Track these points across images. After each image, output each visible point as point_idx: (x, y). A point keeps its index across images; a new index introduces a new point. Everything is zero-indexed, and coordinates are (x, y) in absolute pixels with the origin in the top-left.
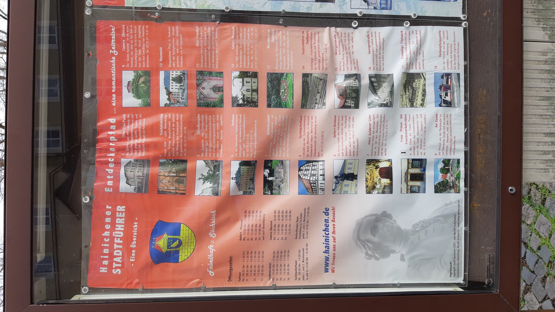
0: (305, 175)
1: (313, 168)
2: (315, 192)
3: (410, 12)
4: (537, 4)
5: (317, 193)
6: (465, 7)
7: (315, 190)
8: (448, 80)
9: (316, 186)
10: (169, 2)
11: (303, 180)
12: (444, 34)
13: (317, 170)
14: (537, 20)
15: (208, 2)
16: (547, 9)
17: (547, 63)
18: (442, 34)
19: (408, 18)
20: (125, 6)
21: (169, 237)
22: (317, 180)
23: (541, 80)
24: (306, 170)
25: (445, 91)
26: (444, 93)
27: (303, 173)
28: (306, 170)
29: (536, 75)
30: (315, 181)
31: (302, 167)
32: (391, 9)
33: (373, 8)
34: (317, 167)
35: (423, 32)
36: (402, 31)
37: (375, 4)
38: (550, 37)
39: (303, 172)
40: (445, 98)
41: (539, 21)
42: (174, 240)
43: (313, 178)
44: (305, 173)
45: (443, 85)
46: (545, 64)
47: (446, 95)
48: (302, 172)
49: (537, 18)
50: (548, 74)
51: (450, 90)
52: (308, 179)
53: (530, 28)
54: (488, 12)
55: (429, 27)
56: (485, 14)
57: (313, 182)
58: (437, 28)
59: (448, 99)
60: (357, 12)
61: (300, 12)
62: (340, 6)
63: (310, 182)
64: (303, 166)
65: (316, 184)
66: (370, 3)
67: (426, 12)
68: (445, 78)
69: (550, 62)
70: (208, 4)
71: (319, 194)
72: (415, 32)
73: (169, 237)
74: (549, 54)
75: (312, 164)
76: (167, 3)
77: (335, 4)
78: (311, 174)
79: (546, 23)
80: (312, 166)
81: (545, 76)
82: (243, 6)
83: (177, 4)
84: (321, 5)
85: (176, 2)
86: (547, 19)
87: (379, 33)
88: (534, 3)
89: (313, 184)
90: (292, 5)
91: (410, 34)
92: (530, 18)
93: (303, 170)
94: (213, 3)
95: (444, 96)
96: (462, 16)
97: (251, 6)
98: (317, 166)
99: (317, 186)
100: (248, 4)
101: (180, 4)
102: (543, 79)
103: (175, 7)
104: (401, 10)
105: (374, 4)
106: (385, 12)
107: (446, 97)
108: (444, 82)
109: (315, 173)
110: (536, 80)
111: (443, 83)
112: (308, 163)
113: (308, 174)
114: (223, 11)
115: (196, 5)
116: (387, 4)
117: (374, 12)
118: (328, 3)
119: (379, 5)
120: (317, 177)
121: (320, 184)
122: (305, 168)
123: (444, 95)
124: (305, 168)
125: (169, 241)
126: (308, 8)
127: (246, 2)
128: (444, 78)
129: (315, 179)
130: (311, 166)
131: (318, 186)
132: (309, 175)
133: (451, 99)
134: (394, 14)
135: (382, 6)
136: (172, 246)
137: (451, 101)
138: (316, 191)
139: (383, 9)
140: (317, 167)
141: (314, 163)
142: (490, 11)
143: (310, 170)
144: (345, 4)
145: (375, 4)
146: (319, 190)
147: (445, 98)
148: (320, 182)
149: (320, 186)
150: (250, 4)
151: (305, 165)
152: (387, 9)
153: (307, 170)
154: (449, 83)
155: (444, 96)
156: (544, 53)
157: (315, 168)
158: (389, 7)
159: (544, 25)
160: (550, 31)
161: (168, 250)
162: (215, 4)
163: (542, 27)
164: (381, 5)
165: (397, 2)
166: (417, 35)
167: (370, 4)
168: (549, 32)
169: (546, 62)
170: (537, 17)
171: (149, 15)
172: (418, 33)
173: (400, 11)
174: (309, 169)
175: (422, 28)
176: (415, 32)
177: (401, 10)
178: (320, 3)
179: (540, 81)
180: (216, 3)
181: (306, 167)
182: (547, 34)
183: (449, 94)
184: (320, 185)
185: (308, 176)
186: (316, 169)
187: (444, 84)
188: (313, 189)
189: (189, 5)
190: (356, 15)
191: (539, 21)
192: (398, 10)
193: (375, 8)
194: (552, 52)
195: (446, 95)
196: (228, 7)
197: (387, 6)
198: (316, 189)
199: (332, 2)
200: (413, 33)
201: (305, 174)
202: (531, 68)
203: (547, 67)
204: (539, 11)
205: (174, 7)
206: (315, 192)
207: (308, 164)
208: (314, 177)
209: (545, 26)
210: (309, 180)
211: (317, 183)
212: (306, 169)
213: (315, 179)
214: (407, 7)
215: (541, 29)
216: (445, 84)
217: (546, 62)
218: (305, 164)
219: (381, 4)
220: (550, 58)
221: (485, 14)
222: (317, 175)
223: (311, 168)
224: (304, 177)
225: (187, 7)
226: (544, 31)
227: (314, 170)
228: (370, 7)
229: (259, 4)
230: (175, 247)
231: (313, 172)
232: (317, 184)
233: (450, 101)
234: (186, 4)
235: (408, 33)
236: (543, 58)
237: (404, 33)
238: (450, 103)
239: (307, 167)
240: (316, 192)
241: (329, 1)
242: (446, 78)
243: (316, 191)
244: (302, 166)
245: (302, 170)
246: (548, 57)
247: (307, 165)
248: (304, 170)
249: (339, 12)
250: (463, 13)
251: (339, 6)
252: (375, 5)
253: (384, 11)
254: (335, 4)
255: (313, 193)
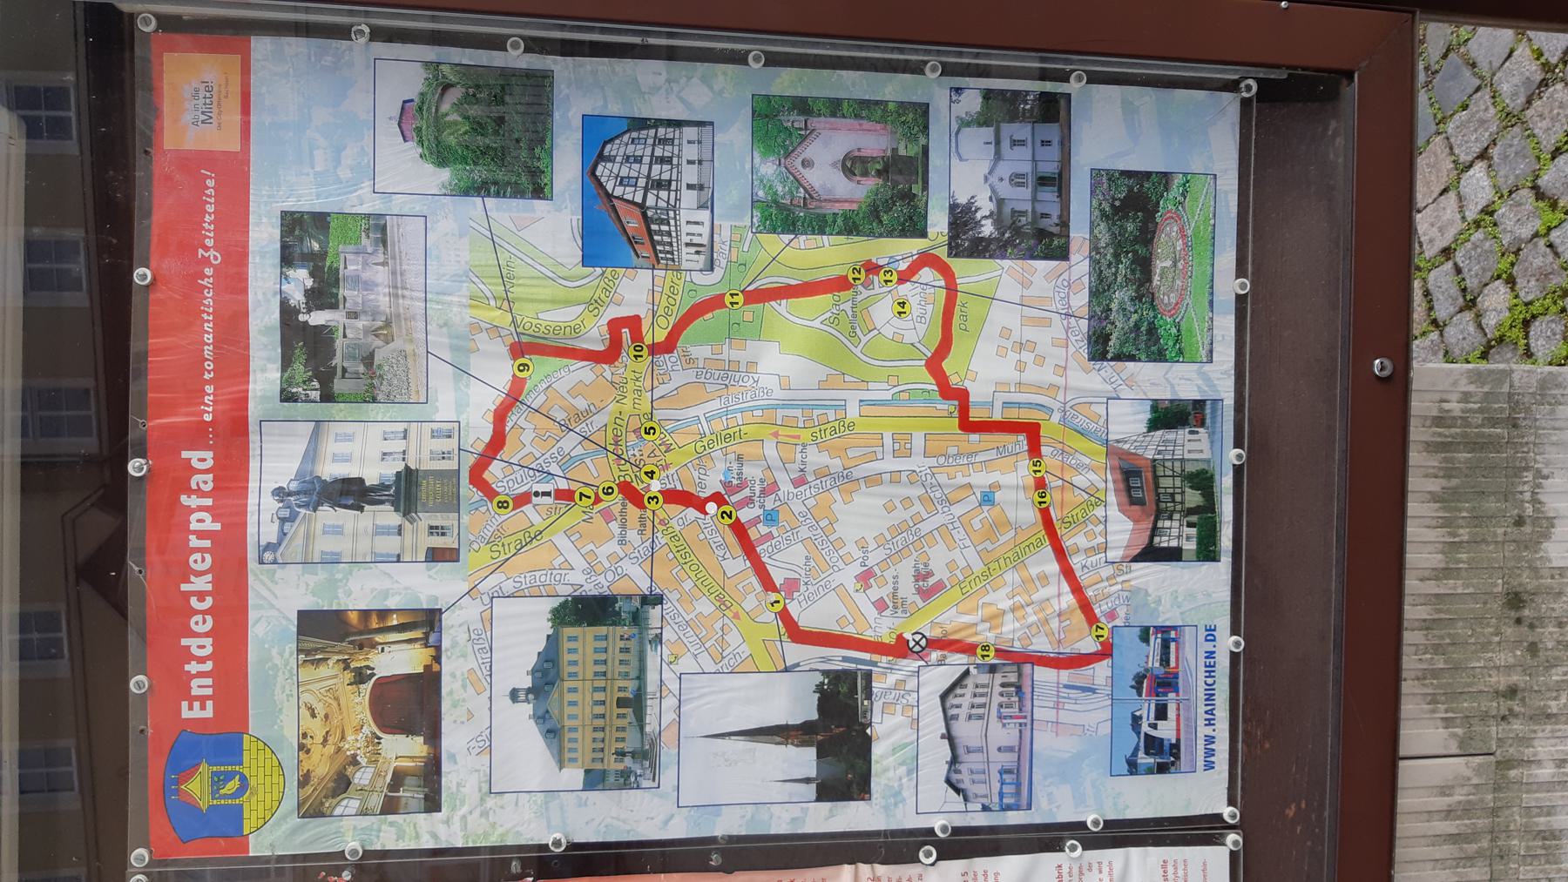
0: (622, 181)
1: (658, 152)
2: (667, 259)
3: (1083, 812)
4: (1431, 654)
5: (673, 260)
6: (1236, 782)
7: (667, 248)
8: (1169, 648)
9: (669, 234)
10: (382, 834)
11: (616, 202)
12: (1176, 868)
13: (675, 161)
14: (1429, 698)
15: (501, 826)
16: (1456, 668)
17: (1452, 814)
18: (1170, 870)
19: (1076, 829)
20: (251, 854)
21: (215, 769)
22: (674, 208)
23: (1432, 863)
24: (627, 158)
25: (1157, 696)
26: (1153, 707)
27: (615, 171)
28: (627, 158)
29: (1422, 851)
30: (667, 210)
31: (608, 147)
32: (1029, 807)
33: (979, 807)
34: (676, 152)
35: (1117, 867)
36: (1060, 866)
37: (986, 796)
38: (1461, 744)
39: (617, 166)
40: (1154, 726)
41: (1434, 700)
42: (229, 777)
43: (657, 196)
44: (624, 172)
45: (1147, 670)
46: (1446, 818)
47: (1161, 713)
48: (609, 165)
49: (1429, 694)
50: (1454, 844)
51: (1177, 692)
52: (639, 199)
53: (1412, 722)
54: (1298, 807)
55: (1135, 852)
56: (1291, 812)
57: (656, 216)
58: (1156, 854)
59: (1166, 731)
60: (938, 824)
61: (772, 832)
62: (886, 808)
63: (644, 215)
64: (617, 141)
65: (668, 224)
66: (970, 794)
67: (1127, 807)
68: (1155, 641)
69: (1459, 813)
70: (500, 830)
71: (685, 265)
72: (1095, 866)
73: (215, 769)
74: (1458, 790)
75: (652, 132)
76: (378, 837)
77: (871, 806)
78: (648, 177)
79: (1455, 705)
80: (654, 145)
81: (1446, 851)
82: (604, 829)
83: (407, 837)
84: (831, 810)
85: (404, 831)
86: (1453, 696)
87: (997, 874)
88: (1424, 653)
89: (659, 224)
90: (749, 816)
91: (1081, 873)
92: (1411, 697)
93: (615, 157)
94: (515, 826)
95: (1152, 720)
96: (1227, 812)
97: (628, 828)
98: (673, 144)
99: (674, 234)
100: (621, 824)
101: (417, 837)
102: (1437, 860)
103: (402, 846)
104: (1058, 807)
105: (981, 797)
106: (1014, 818)
107: (1159, 722)
108: (1151, 658)
109: (666, 176)
110: (1421, 864)
111: (1147, 663)
112: (639, 129)
113: (637, 178)
114: (545, 847)
115: (466, 837)
116: (1018, 793)
117: (981, 820)
118: (852, 803)
119: (996, 799)
120: (673, 194)
121: (688, 222)
122: (622, 150)
123: (1152, 715)
124: (622, 150)
125: (216, 779)
126: (793, 819)
127: (613, 818)
128: (1152, 639)
129: (668, 202)
130: (650, 141)
131: (677, 231)
132: (642, 182)
133: (1178, 730)
134: (1038, 820)
135: (1005, 801)
136: (222, 792)
137: (1178, 740)
138: (668, 252)
139: (1008, 808)
140: (676, 152)
141: (661, 131)
142: (1303, 806)
143: (646, 160)
144: (901, 802)
145: (986, 796)
146: (685, 250)
147: (1154, 726)
148: (684, 216)
149: (688, 234)
150: (624, 821)
151: (626, 138)
152: (1016, 807)
153: (632, 160)
154: (1173, 664)
155: (1152, 720)
156: (1445, 790)
157: (666, 154)
158: (1024, 801)
159: (1446, 711)
160: (1462, 726)
161: (215, 802)
162: (520, 829)
163: (1442, 718)
164: (1001, 799)
165: (1049, 786)
166: (1101, 876)
167: (971, 799)
168: (1459, 731)
169: (1448, 813)
170: (1430, 691)
171: (324, 877)
172: (1105, 869)
173: (1055, 810)
174: (642, 157)
175: (1115, 856)
176: (1095, 866)
177: (1058, 807)
178: (829, 804)
179: (1429, 865)
180: (525, 826)
181: (627, 144)
182: (1454, 735)
183: (1172, 713)
184: (685, 229)
185: (636, 186)
186: (671, 158)
187: (1150, 665)
188: (660, 243)
189: (443, 838)
190: (931, 831)
191: (1434, 701)
192: (1051, 810)
193: (985, 808)
194: (1463, 786)
195: (1161, 713)
196: (560, 840)
197: (1019, 800)
198: (671, 244)
199: (863, 799)
200: (1090, 869)
201: (622, 178)
202: (1409, 835)
203: (1449, 827)
204: (1435, 673)
205: (397, 845)
206: (667, 259)
207: (634, 135)
208: (664, 194)
209: (1450, 715)
210: (642, 206)
211: (675, 218)
212: (628, 157)
213: (668, 202)
214: (1074, 797)
215: (1439, 723)
216: (1157, 664)
217: (1448, 813)
218: (625, 133)
219: (1001, 795)
220: (1460, 802)
221: (1291, 812)
222: (674, 183)
223: (648, 151)
224: (618, 191)
225: (436, 843)
226: (1446, 728)
227: (663, 160)
228: (970, 807)
229: (652, 819)
230: (233, 796)
231: (656, 168)
232: (676, 226)
233: (1174, 741)
234: (435, 836)
235: (1075, 871)
236: (1442, 802)
237: (1065, 870)
238: (1175, 748)
239: (631, 148)
240: (669, 256)
241: (855, 797)
242: (1159, 641)
243: (668, 252)
244: (611, 140)
245: (611, 159)
246: (1457, 798)
247: (633, 139)
248: (619, 159)
249: (883, 827)
250: (1231, 802)
251: (882, 810)
252: (985, 801)
253: (1009, 813)
254: (871, 806)
255: (659, 262)
